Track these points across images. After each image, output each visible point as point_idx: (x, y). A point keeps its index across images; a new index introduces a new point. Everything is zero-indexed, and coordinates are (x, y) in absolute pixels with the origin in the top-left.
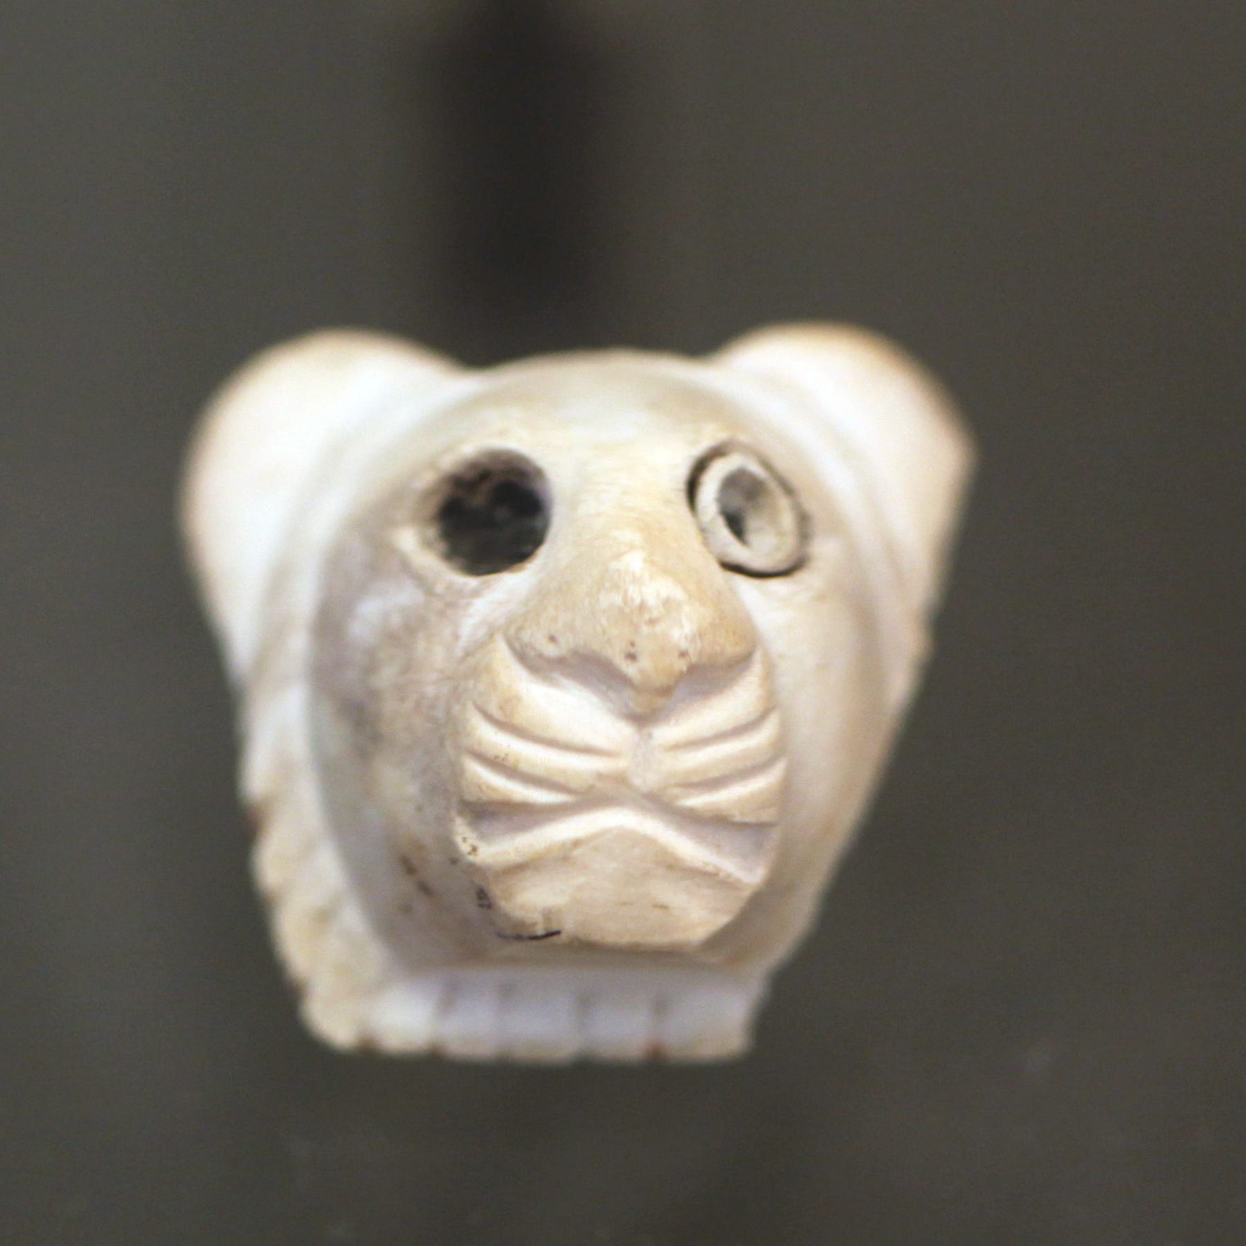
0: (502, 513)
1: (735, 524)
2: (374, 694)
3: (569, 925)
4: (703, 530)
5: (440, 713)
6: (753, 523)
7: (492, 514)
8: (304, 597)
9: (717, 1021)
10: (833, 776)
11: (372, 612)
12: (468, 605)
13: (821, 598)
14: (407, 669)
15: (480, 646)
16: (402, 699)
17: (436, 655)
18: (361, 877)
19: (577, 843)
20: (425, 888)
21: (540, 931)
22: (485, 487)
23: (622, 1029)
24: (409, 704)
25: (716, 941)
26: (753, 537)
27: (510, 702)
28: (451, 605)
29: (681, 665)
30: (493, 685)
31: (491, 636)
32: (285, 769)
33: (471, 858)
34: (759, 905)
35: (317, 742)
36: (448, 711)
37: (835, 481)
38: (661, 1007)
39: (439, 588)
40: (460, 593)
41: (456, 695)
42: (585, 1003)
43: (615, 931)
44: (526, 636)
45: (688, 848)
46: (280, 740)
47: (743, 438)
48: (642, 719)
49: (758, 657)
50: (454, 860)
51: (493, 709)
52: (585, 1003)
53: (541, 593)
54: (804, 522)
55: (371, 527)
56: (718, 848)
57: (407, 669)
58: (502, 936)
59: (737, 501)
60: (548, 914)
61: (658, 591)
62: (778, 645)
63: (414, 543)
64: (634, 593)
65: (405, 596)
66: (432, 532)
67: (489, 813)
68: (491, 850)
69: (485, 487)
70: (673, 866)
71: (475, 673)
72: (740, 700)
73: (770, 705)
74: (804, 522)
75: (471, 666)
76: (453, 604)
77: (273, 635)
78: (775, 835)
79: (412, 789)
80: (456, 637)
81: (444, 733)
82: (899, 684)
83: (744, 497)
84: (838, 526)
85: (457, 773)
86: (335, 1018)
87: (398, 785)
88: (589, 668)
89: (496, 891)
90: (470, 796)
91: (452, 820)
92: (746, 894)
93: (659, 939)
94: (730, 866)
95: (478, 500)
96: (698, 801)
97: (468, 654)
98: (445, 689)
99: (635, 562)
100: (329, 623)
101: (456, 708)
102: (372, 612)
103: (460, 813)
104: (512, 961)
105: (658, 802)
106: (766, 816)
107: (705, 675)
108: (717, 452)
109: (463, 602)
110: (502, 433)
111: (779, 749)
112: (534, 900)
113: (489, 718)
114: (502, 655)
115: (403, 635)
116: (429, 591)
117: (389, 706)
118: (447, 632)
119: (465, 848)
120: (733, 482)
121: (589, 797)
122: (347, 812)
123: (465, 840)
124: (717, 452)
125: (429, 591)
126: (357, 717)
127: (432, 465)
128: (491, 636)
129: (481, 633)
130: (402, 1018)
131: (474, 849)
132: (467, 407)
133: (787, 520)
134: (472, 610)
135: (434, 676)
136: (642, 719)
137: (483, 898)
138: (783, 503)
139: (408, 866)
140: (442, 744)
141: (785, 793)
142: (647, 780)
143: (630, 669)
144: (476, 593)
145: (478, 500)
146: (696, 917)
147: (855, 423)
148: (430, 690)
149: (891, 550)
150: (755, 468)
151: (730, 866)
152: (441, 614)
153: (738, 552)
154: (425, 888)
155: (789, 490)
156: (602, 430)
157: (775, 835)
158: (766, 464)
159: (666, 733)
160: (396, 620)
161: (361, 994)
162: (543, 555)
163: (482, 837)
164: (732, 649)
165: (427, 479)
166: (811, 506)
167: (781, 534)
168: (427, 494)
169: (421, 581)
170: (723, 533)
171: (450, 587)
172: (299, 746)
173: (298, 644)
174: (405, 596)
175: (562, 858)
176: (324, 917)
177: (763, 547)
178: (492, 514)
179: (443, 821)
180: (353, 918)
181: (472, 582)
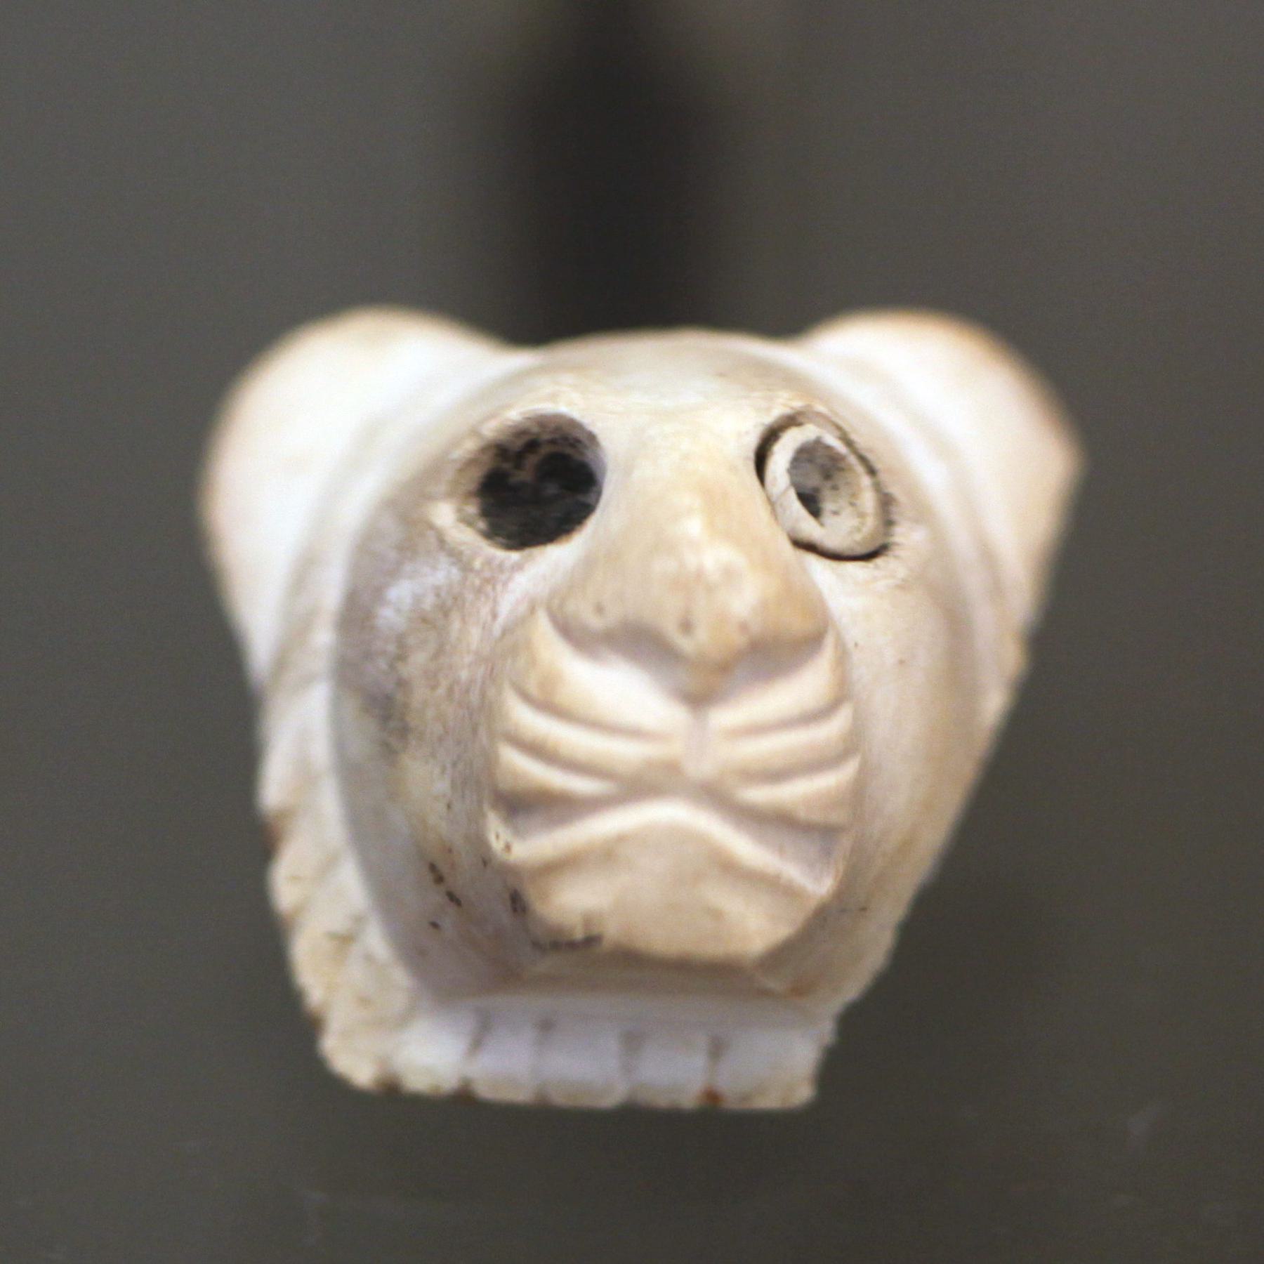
0: (551, 489)
1: (811, 502)
2: (402, 684)
3: (612, 931)
4: (771, 503)
5: (474, 698)
6: (828, 506)
7: (538, 485)
8: (330, 590)
9: (780, 1064)
10: (918, 804)
11: (402, 597)
12: (509, 579)
13: (903, 586)
14: (439, 652)
15: (521, 622)
16: (434, 688)
17: (472, 636)
18: (386, 896)
19: (621, 839)
20: (453, 898)
21: (579, 935)
22: (532, 460)
23: (674, 1073)
24: (441, 691)
25: (778, 957)
26: (827, 518)
27: (551, 681)
28: (490, 581)
29: (740, 640)
30: (533, 662)
31: (532, 610)
32: (305, 777)
33: (505, 857)
34: (826, 923)
35: (339, 745)
36: (483, 695)
37: (927, 472)
38: (717, 1050)
39: (477, 564)
40: (501, 567)
41: (492, 676)
42: (633, 1041)
43: (664, 938)
44: (571, 607)
45: (746, 848)
46: (300, 744)
47: (820, 408)
48: (699, 699)
49: (829, 641)
50: (485, 860)
51: (532, 688)
52: (633, 1041)
53: (589, 563)
54: (886, 502)
55: (405, 509)
56: (781, 851)
57: (439, 652)
58: (537, 945)
59: (813, 480)
60: (588, 920)
61: (714, 557)
62: (854, 633)
63: (450, 517)
64: (691, 561)
65: (442, 574)
66: (472, 509)
67: (525, 805)
68: (524, 847)
69: (532, 460)
70: (729, 869)
71: (514, 651)
72: (807, 685)
73: (841, 695)
74: (886, 502)
75: (511, 642)
76: (492, 580)
77: (296, 632)
78: (846, 842)
79: (442, 786)
80: (494, 616)
81: (478, 720)
82: (993, 703)
83: (821, 470)
84: (925, 515)
85: (490, 761)
86: (353, 1056)
87: (426, 779)
88: (639, 642)
89: (531, 894)
90: (505, 784)
91: (484, 816)
92: (812, 904)
93: (712, 949)
94: (793, 871)
95: (525, 475)
96: (759, 795)
97: (505, 631)
98: (481, 672)
99: (694, 526)
100: (356, 615)
101: (491, 692)
102: (402, 597)
103: (494, 806)
104: (551, 982)
105: (714, 795)
106: (837, 817)
107: (771, 651)
108: (791, 421)
109: (503, 577)
110: (553, 397)
111: (851, 745)
112: (573, 902)
113: (526, 697)
114: (543, 629)
115: (435, 619)
116: (466, 568)
117: (420, 693)
118: (485, 611)
119: (497, 845)
120: (806, 455)
121: (636, 786)
122: (367, 826)
123: (497, 837)
124: (791, 421)
125: (466, 568)
126: (382, 708)
127: (474, 432)
128: (532, 610)
129: (523, 608)
130: (431, 1055)
131: (508, 847)
132: (516, 379)
133: (868, 500)
134: (511, 586)
135: (468, 659)
136: (699, 699)
137: (517, 903)
138: (866, 481)
139: (433, 868)
140: (475, 731)
141: (857, 794)
142: (702, 768)
143: (686, 644)
144: (518, 567)
145: (525, 475)
146: (754, 927)
147: (954, 423)
148: (464, 675)
149: (988, 557)
150: (832, 440)
151: (793, 871)
152: (479, 591)
153: (810, 528)
154: (453, 898)
155: (872, 471)
156: (667, 411)
157: (846, 842)
158: (849, 443)
159: (725, 717)
160: (429, 602)
161: (386, 1030)
162: (592, 524)
163: (518, 833)
164: (797, 624)
165: (470, 446)
166: (894, 490)
167: (862, 515)
168: (471, 462)
169: (456, 556)
170: (797, 507)
171: (488, 562)
172: (321, 751)
173: (324, 637)
174: (442, 574)
175: (606, 855)
176: (344, 940)
177: (839, 528)
178: (538, 485)
179: (476, 818)
180: (375, 940)
181: (515, 556)
